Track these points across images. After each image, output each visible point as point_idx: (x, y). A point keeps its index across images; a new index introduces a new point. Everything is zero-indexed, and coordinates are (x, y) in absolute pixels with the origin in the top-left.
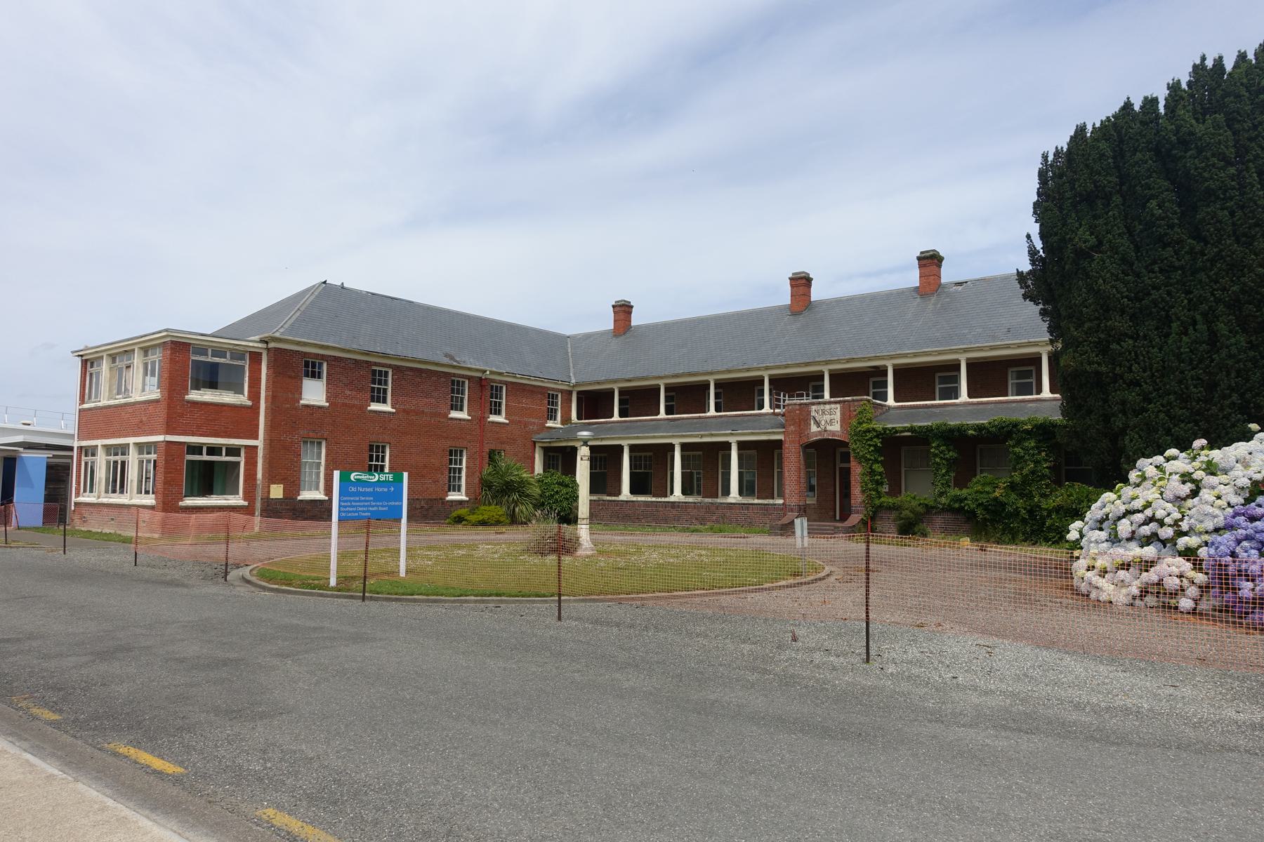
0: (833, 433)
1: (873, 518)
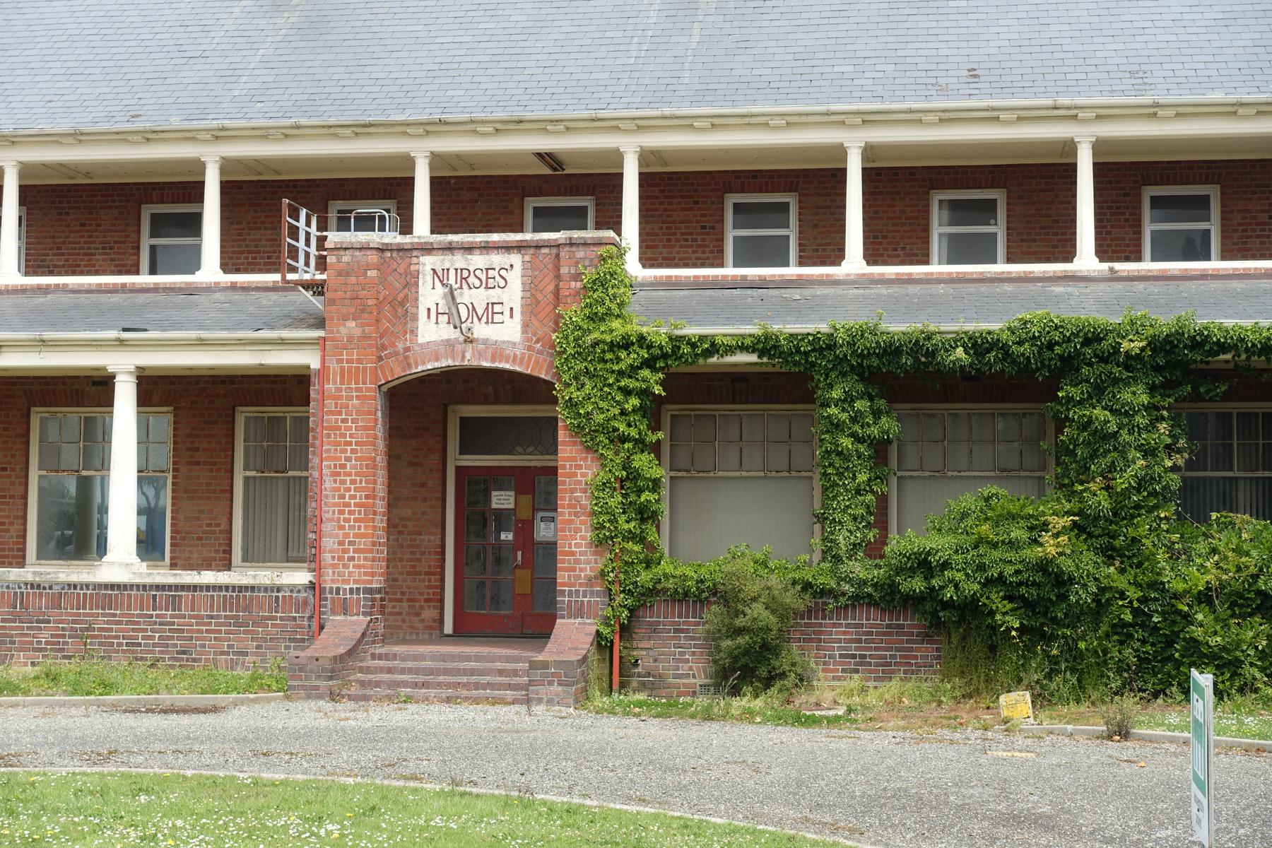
0: (497, 350)
1: (626, 631)
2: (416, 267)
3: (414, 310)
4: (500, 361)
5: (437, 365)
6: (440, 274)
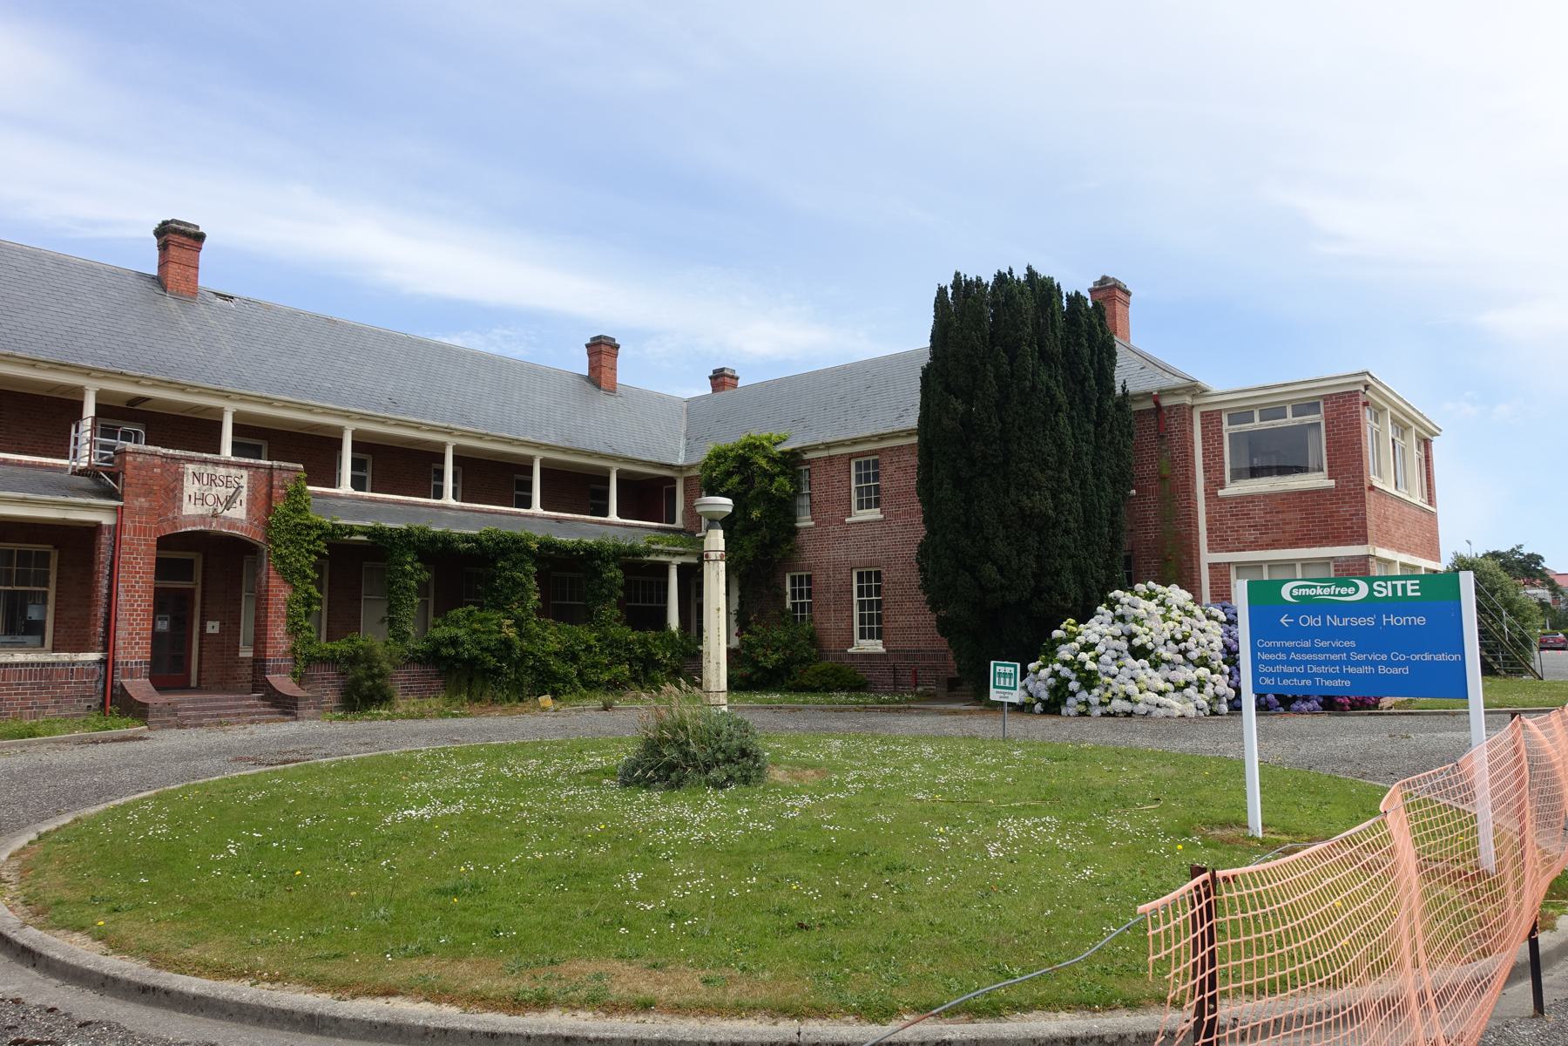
0: (232, 523)
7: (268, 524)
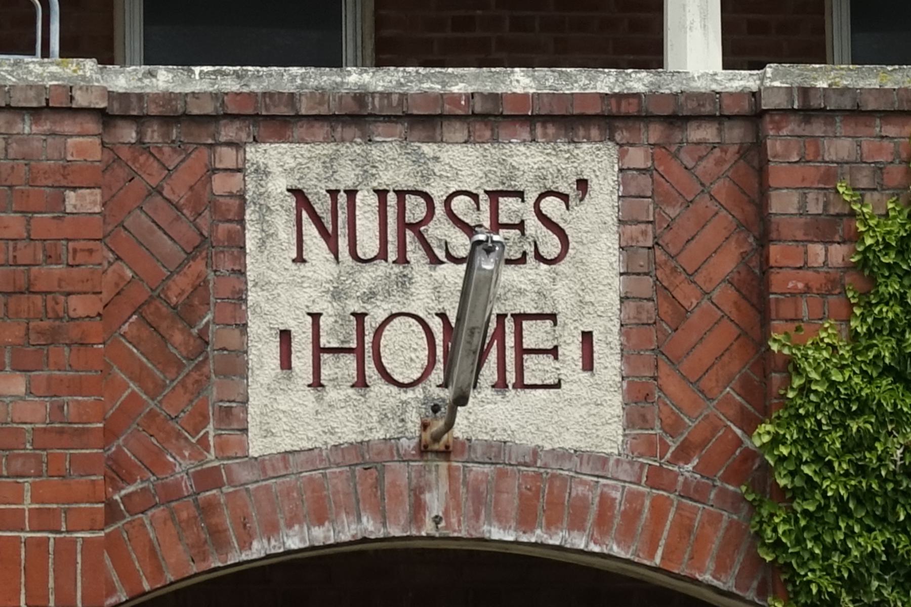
0: (540, 481)
2: (234, 183)
3: (231, 337)
4: (551, 525)
5: (321, 535)
6: (322, 207)
7: (753, 471)
